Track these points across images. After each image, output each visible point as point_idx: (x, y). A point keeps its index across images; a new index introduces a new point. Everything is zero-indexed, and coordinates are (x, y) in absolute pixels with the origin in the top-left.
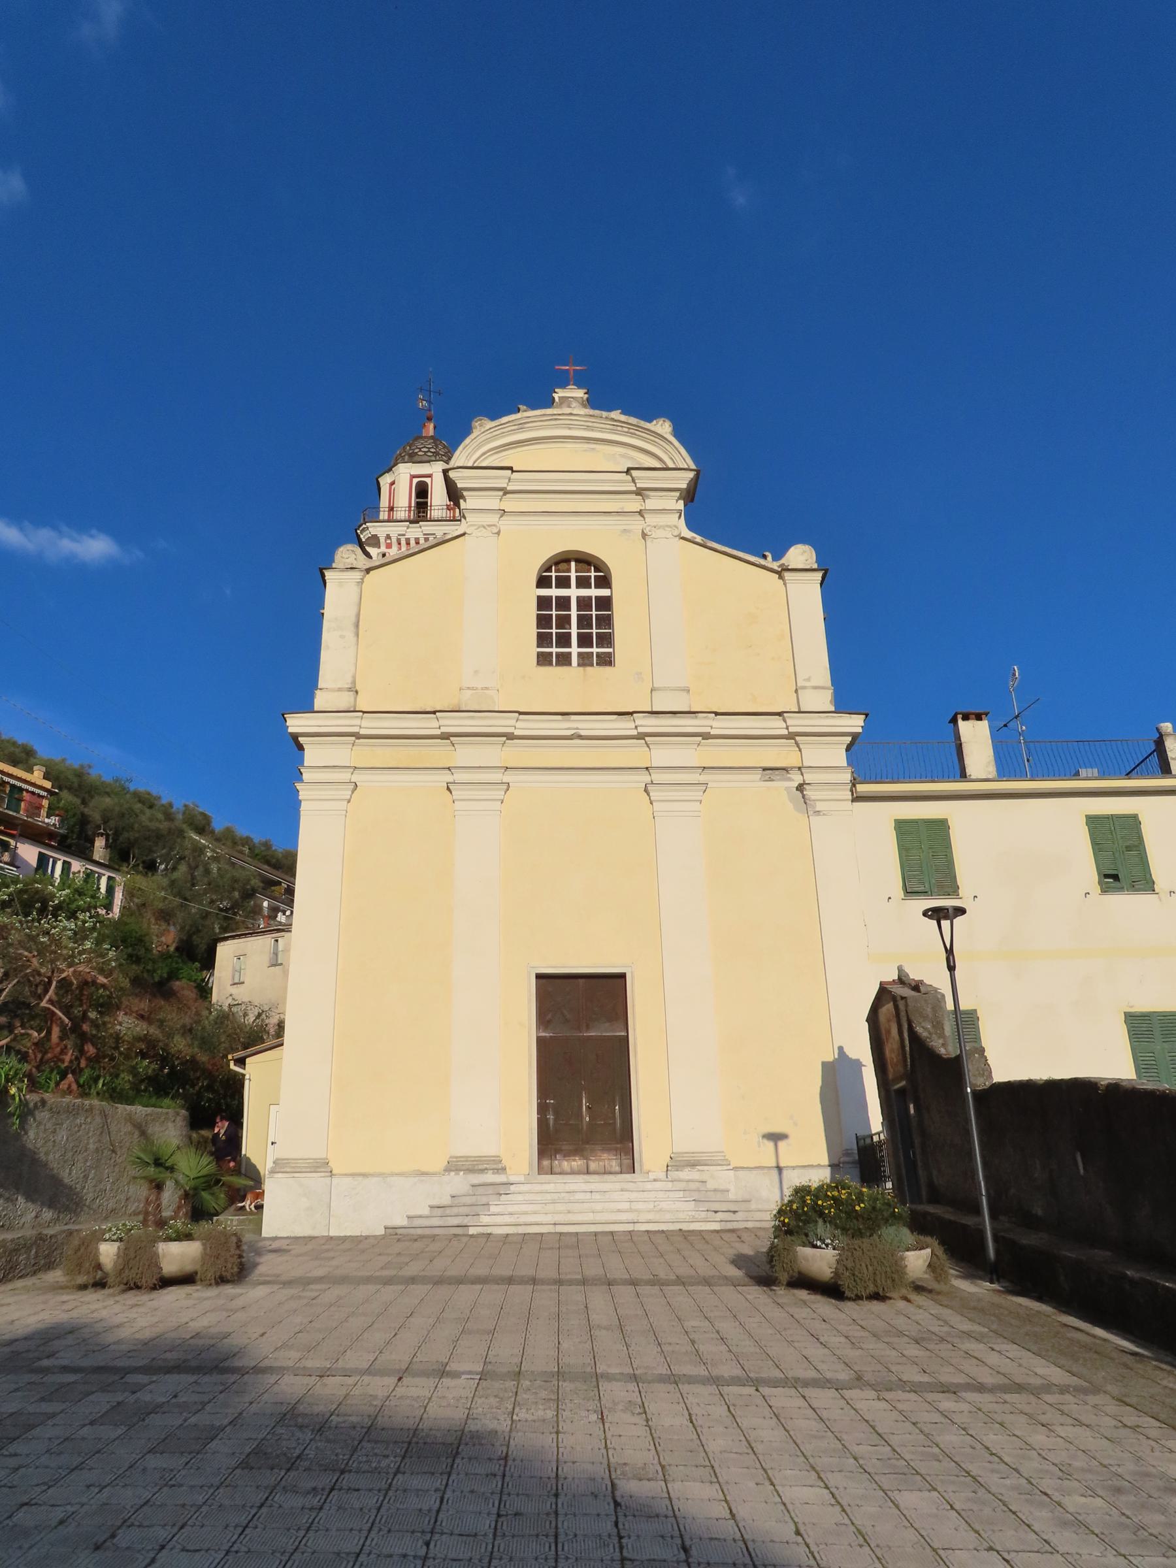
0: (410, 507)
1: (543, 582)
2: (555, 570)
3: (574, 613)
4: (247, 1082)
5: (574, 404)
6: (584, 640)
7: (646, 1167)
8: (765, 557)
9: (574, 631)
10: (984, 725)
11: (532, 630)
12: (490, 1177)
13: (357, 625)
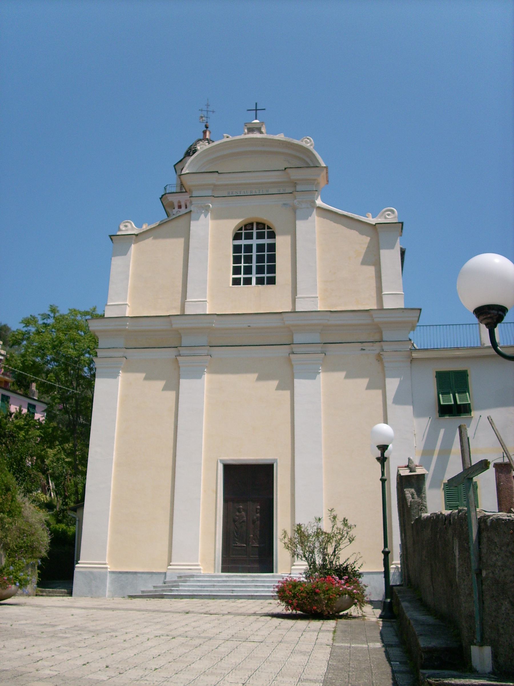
1: (237, 236)
6: (260, 270)
9: (254, 265)
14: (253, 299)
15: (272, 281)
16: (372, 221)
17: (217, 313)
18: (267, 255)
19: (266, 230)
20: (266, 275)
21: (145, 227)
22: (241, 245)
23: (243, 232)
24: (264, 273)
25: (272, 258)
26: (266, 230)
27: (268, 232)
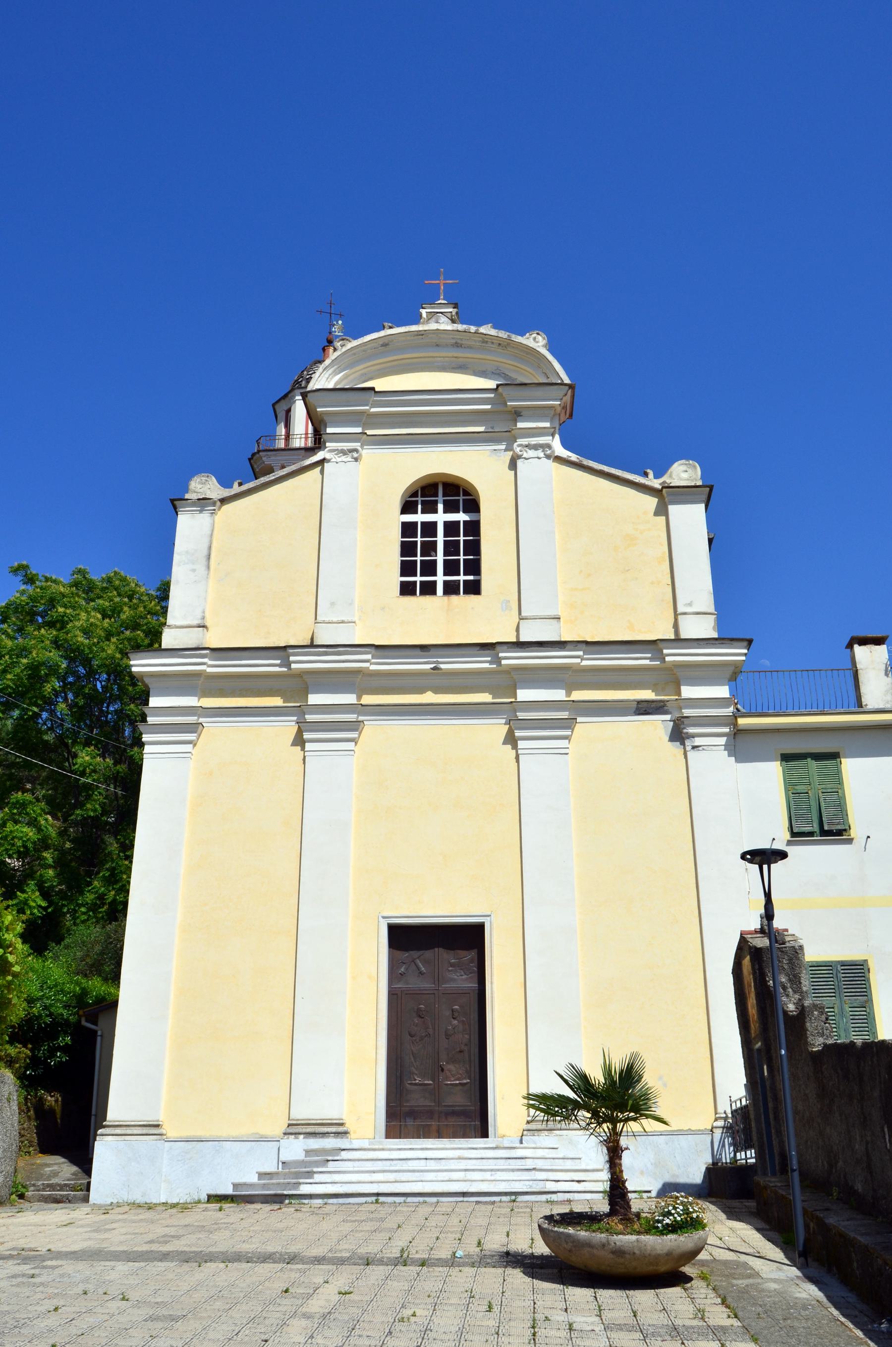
0: (307, 434)
1: (408, 507)
2: (428, 492)
3: (440, 539)
4: (99, 1039)
5: (443, 319)
6: (451, 568)
7: (501, 1130)
8: (646, 475)
9: (440, 558)
10: (881, 651)
11: (395, 558)
12: (330, 1143)
13: (209, 557)
14: (437, 619)
15: (474, 588)
16: (656, 484)
17: (376, 644)
18: (464, 541)
19: (461, 498)
20: (418, 579)
21: (236, 489)
22: (459, 522)
23: (419, 499)
24: (416, 576)
25: (474, 548)
26: (461, 498)
27: (464, 500)
